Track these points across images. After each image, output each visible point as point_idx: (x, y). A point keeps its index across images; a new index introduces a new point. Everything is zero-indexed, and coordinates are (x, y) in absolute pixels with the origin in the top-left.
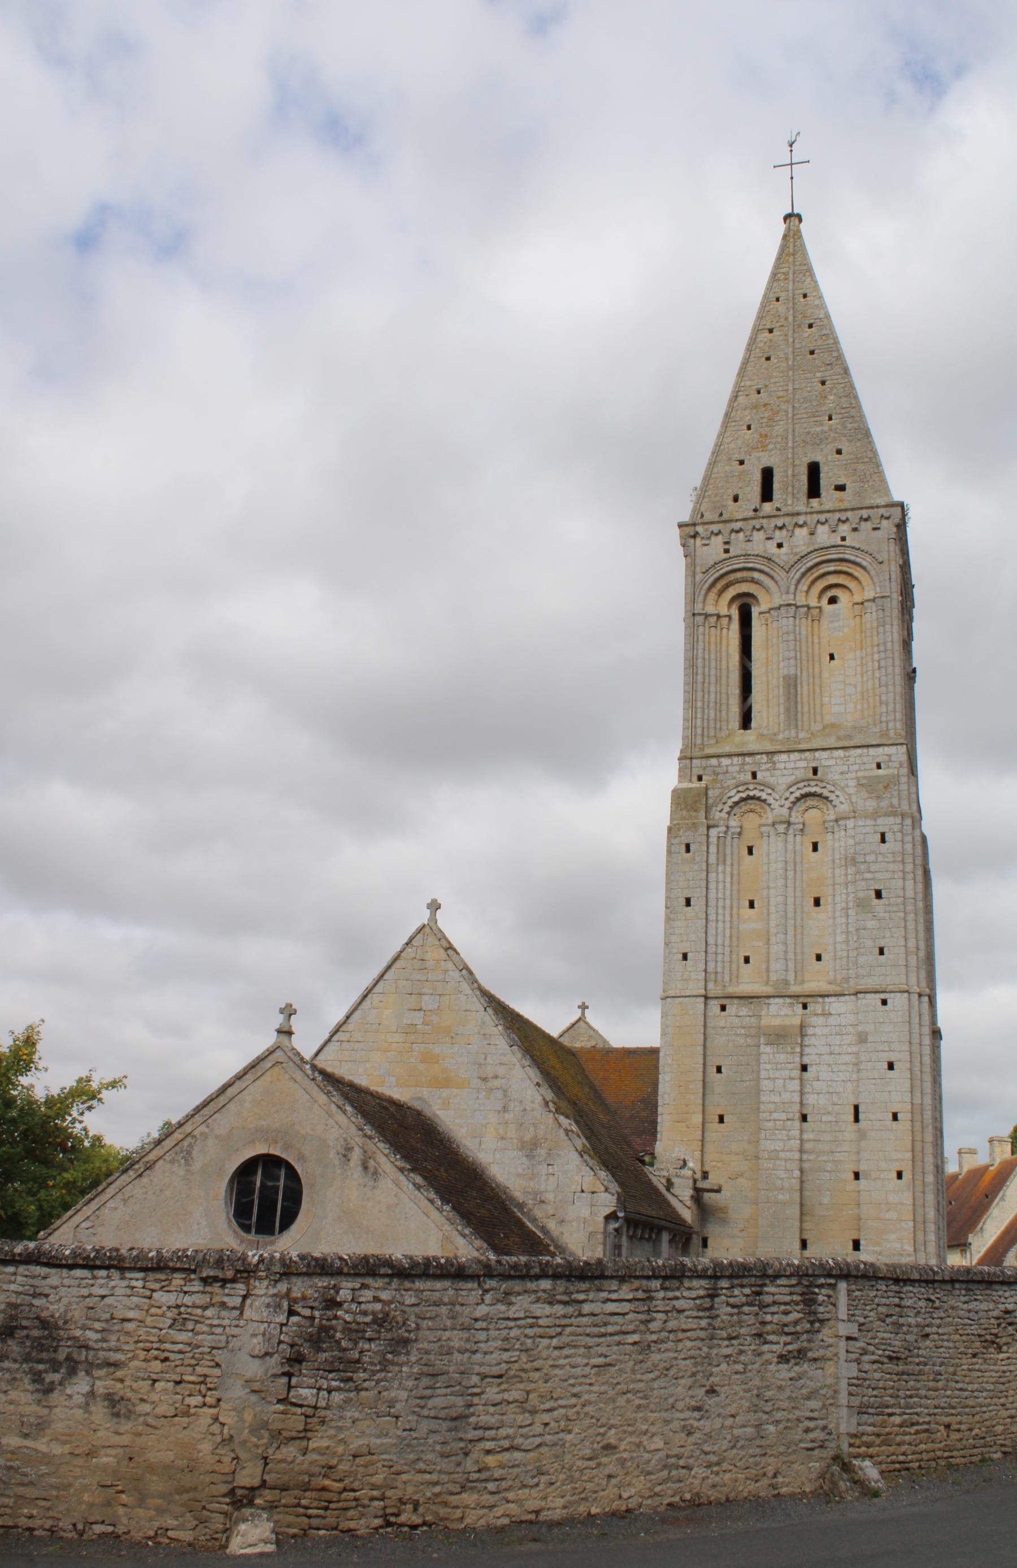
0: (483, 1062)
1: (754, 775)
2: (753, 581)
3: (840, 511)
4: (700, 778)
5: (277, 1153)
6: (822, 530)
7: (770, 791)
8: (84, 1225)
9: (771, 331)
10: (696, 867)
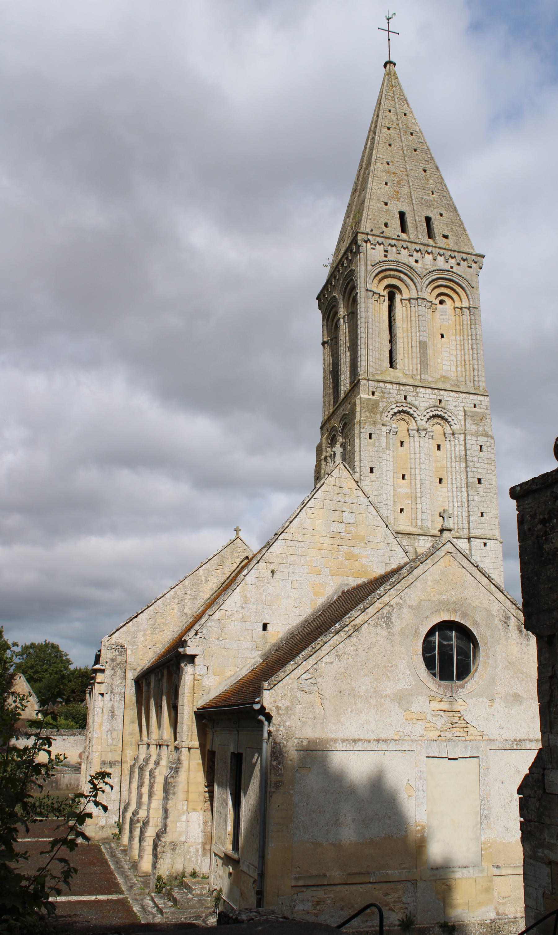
0: (388, 562)
1: (405, 398)
2: (400, 279)
3: (451, 250)
4: (373, 394)
5: (458, 619)
6: (440, 259)
7: (415, 409)
8: (304, 677)
9: (389, 129)
10: (376, 449)
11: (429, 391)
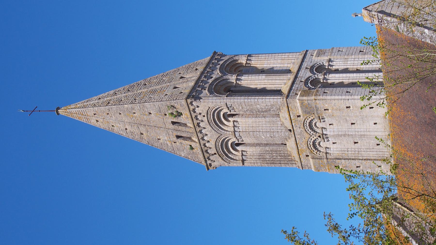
4: (296, 94)
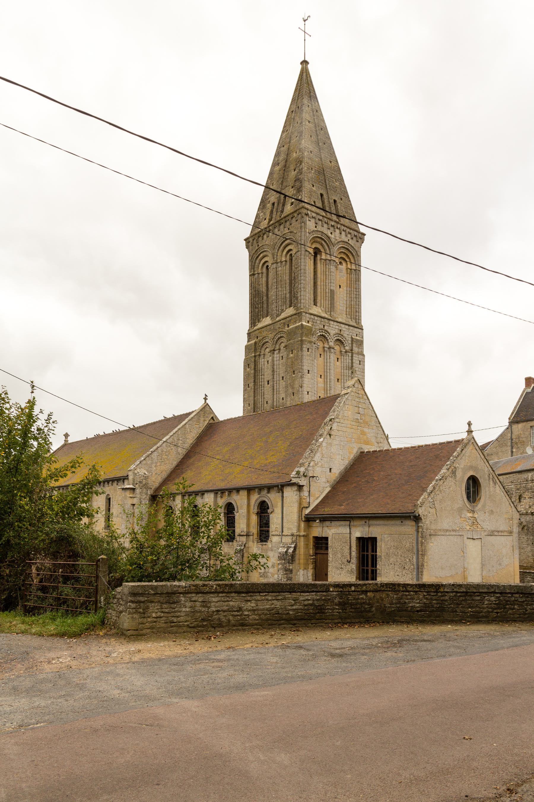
2: (322, 245)
4: (308, 322)
11: (335, 324)
